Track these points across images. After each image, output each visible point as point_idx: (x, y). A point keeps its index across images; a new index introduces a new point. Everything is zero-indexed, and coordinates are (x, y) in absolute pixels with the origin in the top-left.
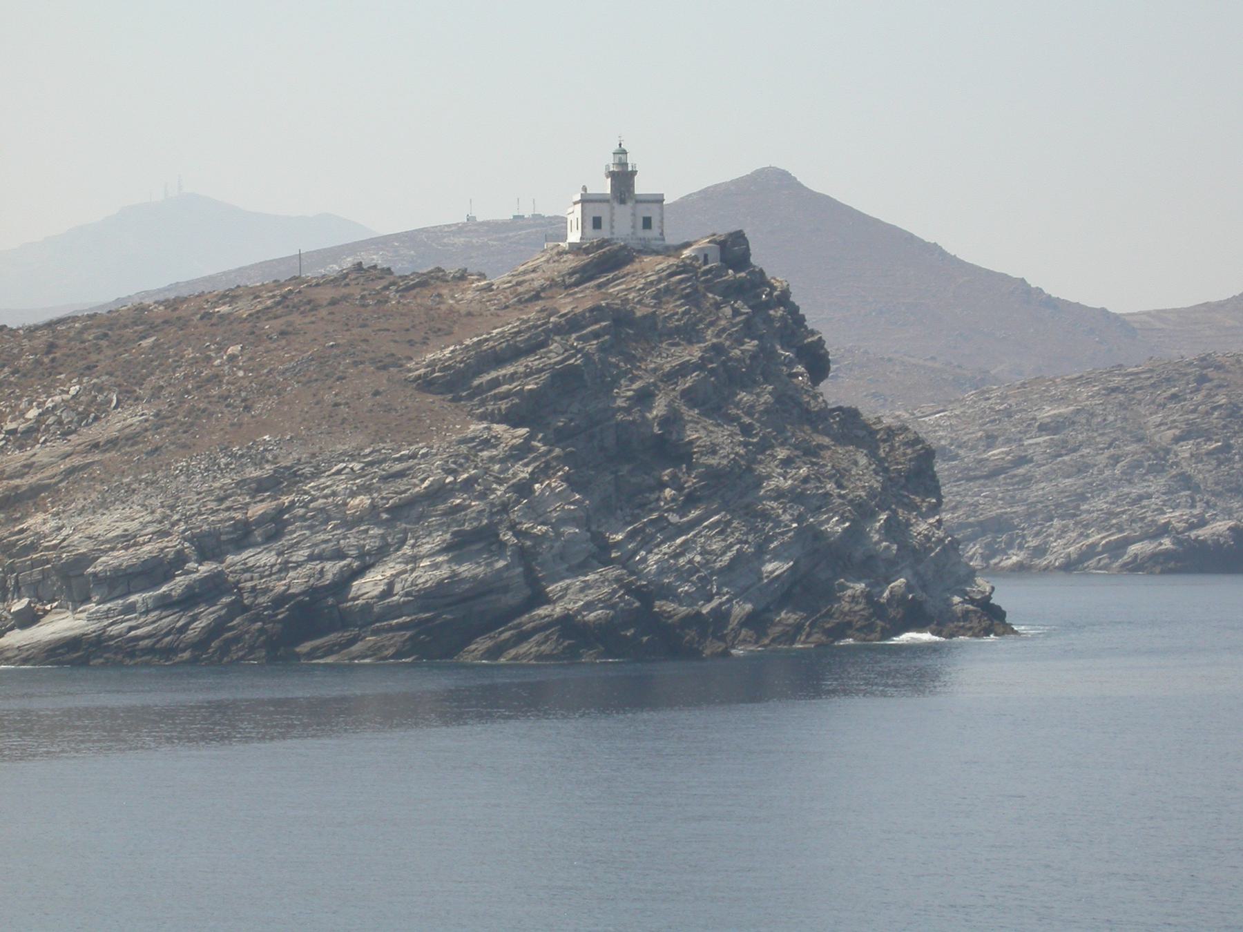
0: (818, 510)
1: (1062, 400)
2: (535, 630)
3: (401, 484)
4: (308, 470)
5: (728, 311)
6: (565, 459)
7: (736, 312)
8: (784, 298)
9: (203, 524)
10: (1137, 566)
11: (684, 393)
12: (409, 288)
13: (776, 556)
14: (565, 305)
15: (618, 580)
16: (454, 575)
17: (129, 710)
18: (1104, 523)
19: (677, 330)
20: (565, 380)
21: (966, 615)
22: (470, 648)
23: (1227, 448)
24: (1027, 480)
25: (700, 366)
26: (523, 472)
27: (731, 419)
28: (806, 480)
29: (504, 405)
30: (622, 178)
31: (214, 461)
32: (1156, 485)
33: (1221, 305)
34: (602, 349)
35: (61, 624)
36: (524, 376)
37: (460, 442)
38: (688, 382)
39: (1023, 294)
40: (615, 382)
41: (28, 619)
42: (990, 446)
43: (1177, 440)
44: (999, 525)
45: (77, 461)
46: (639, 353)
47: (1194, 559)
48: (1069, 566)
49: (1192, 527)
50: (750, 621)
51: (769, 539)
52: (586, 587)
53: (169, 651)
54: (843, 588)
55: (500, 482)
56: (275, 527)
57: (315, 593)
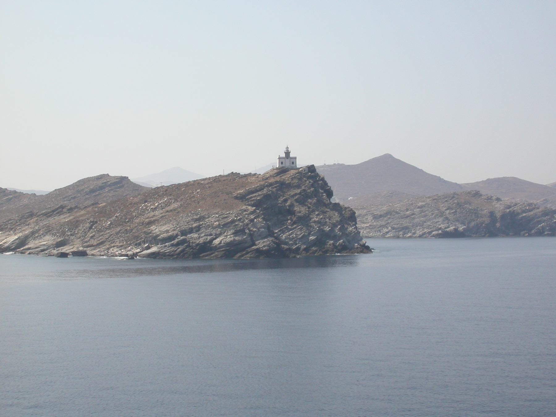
0: (324, 225)
1: (424, 201)
2: (250, 252)
3: (225, 220)
4: (207, 216)
5: (308, 182)
6: (263, 214)
7: (310, 182)
8: (323, 179)
9: (183, 228)
10: (434, 236)
11: (295, 200)
12: (241, 177)
13: (313, 235)
14: (272, 180)
15: (272, 240)
16: (234, 239)
17: (198, 267)
18: (428, 227)
19: (295, 186)
20: (267, 197)
21: (357, 248)
22: (237, 255)
23: (456, 211)
24: (414, 218)
25: (300, 193)
26: (252, 217)
27: (306, 205)
28: (322, 219)
29: (252, 202)
30: (287, 153)
31: (188, 215)
32: (441, 219)
33: (480, 182)
34: (277, 190)
35: (154, 249)
36: (257, 196)
37: (240, 210)
38: (297, 197)
39: (439, 180)
40: (279, 197)
41: (148, 248)
42: (407, 211)
43: (446, 210)
44: (407, 228)
45: (163, 214)
46: (286, 191)
47: (446, 235)
48: (420, 236)
49: (446, 228)
50: (304, 249)
52: (264, 242)
53: (172, 255)
54: (328, 242)
55: (247, 219)
56: (198, 229)
57: (205, 243)
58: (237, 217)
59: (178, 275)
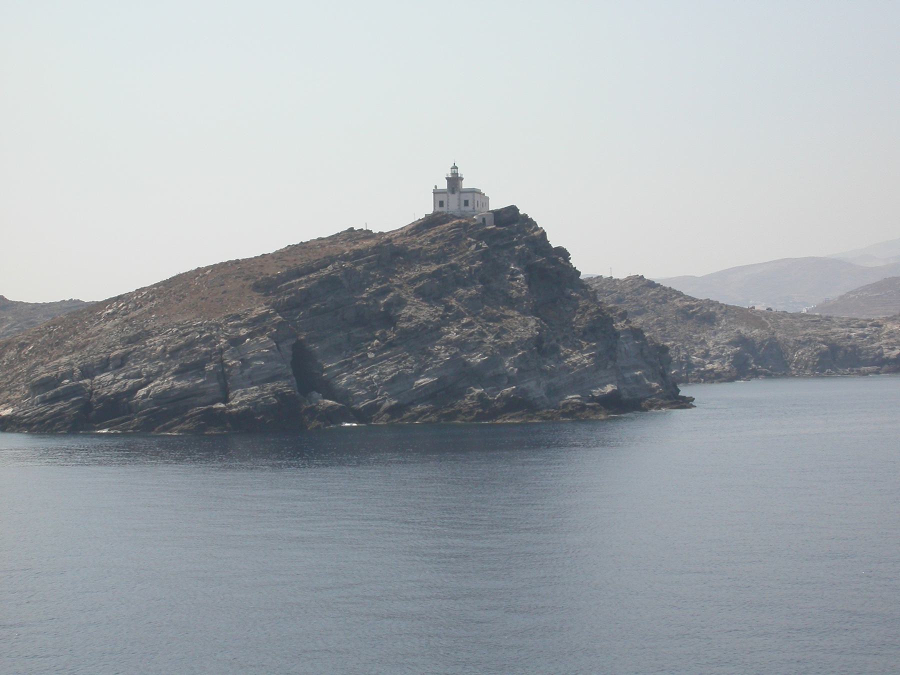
7: (478, 247)
13: (428, 375)
16: (173, 386)
20: (331, 282)
30: (454, 181)
50: (391, 410)
51: (426, 366)
54: (471, 391)
57: (117, 395)
58: (201, 333)
59: (333, 471)
